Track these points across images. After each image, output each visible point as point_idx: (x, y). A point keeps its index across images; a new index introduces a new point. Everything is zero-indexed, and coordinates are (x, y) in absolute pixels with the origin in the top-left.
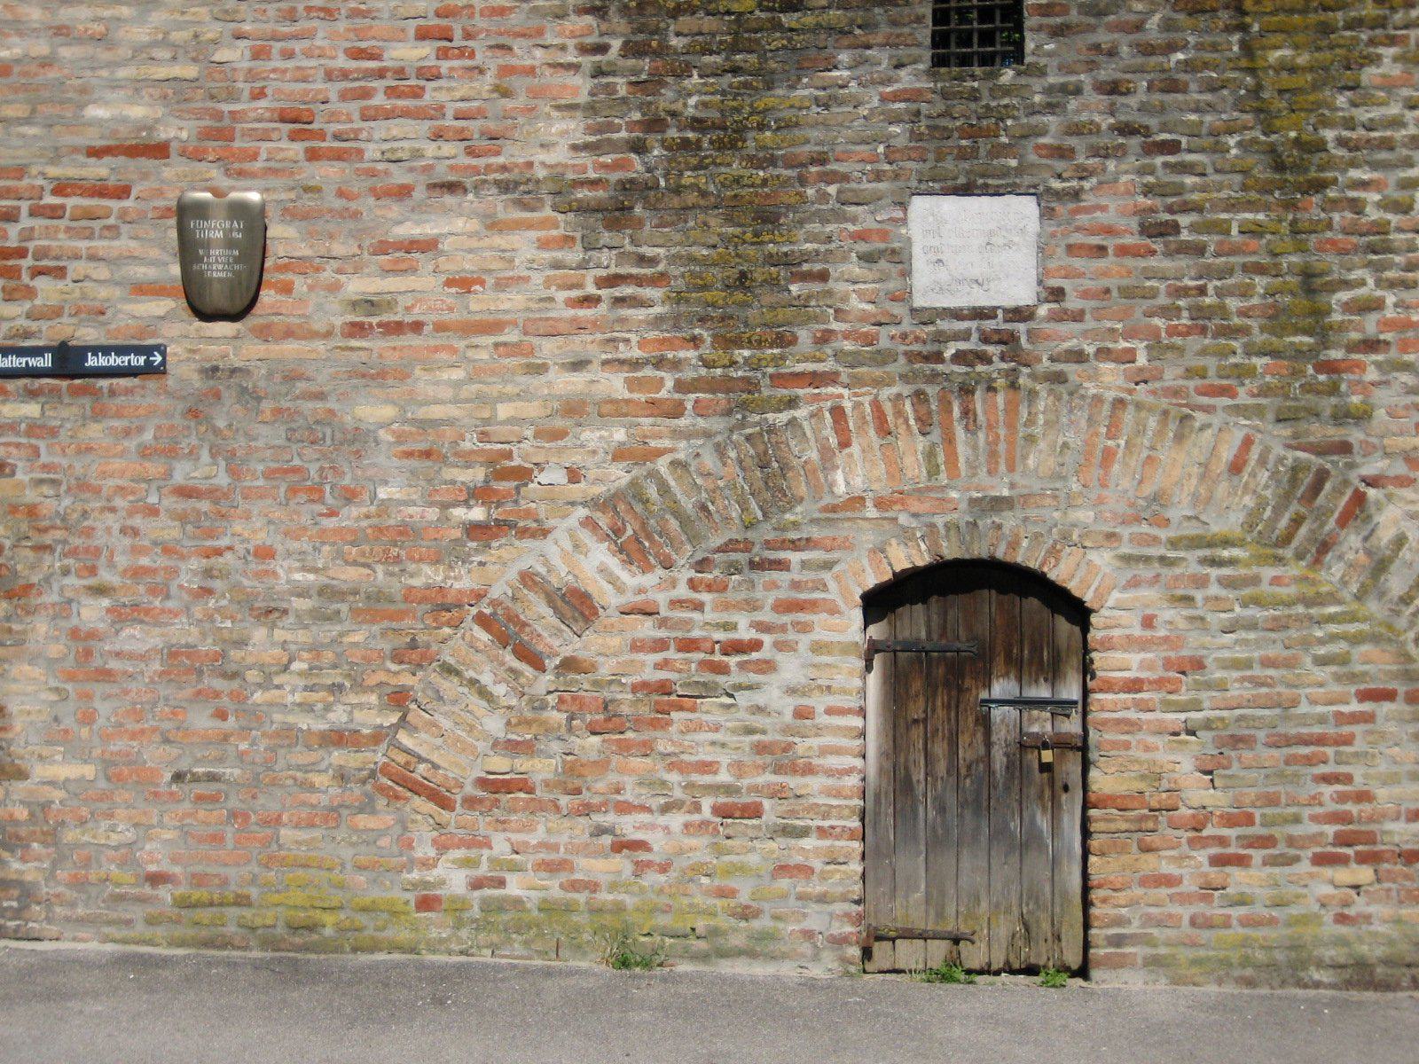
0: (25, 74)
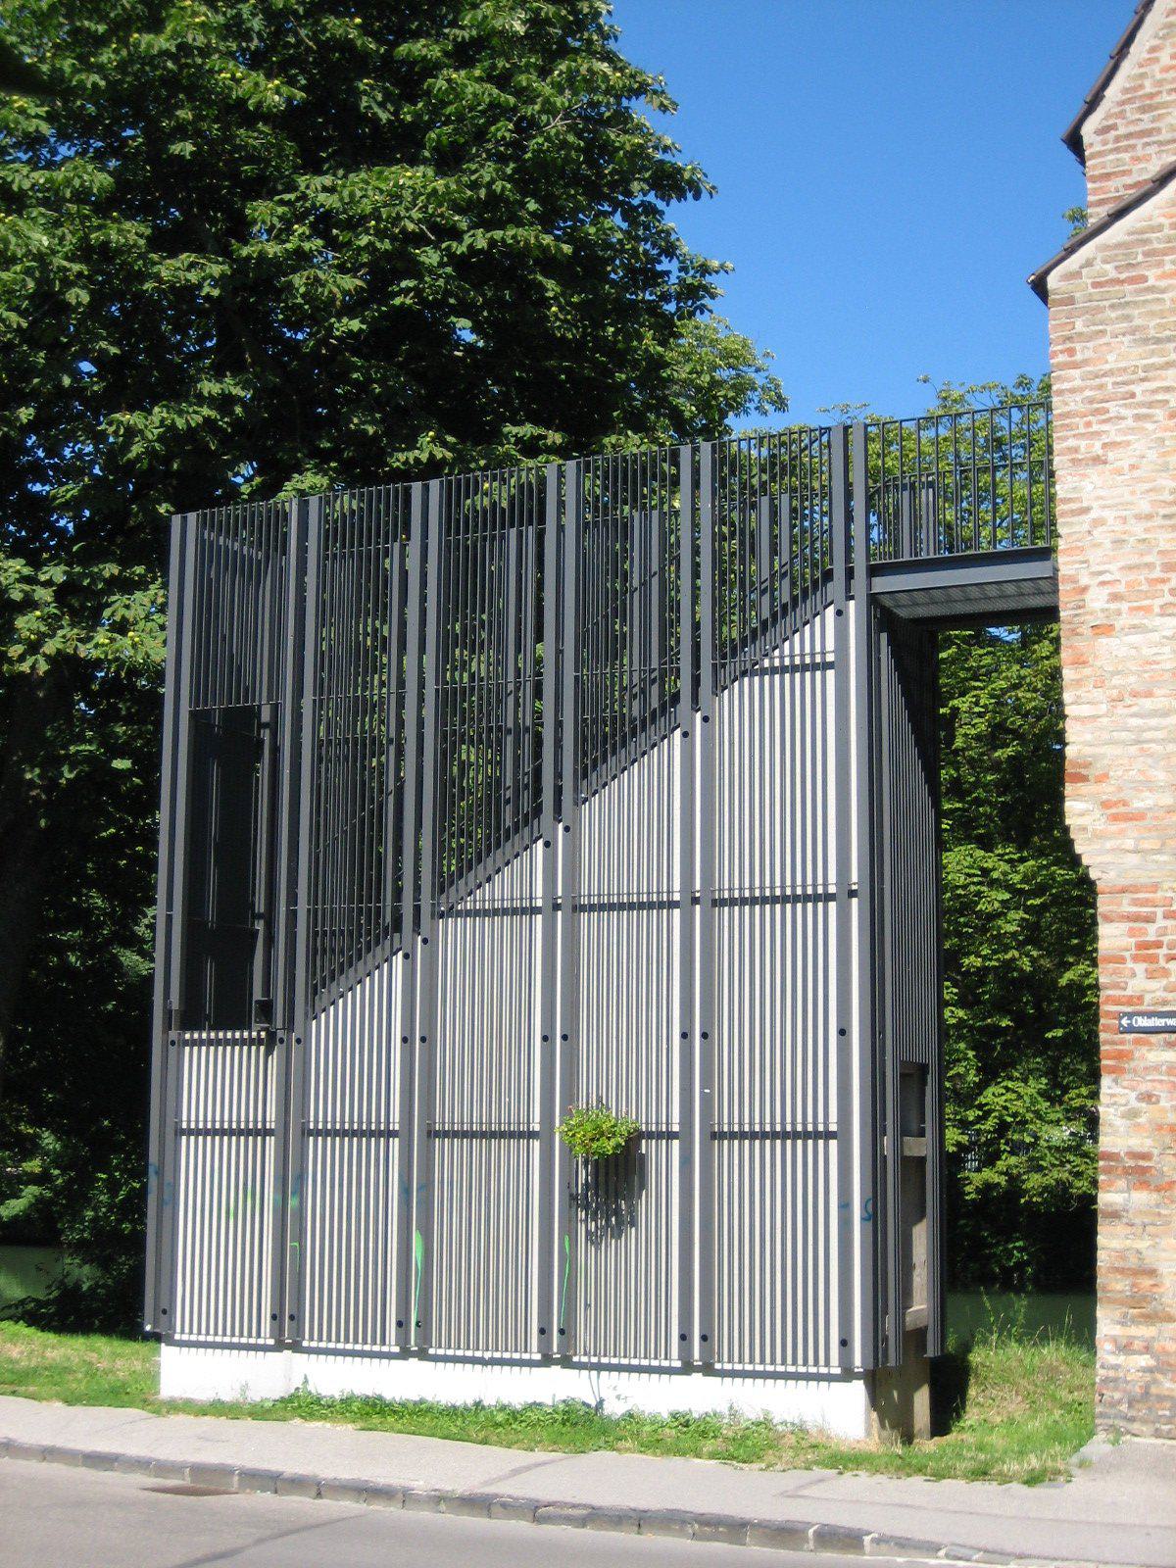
0: (1156, 818)
